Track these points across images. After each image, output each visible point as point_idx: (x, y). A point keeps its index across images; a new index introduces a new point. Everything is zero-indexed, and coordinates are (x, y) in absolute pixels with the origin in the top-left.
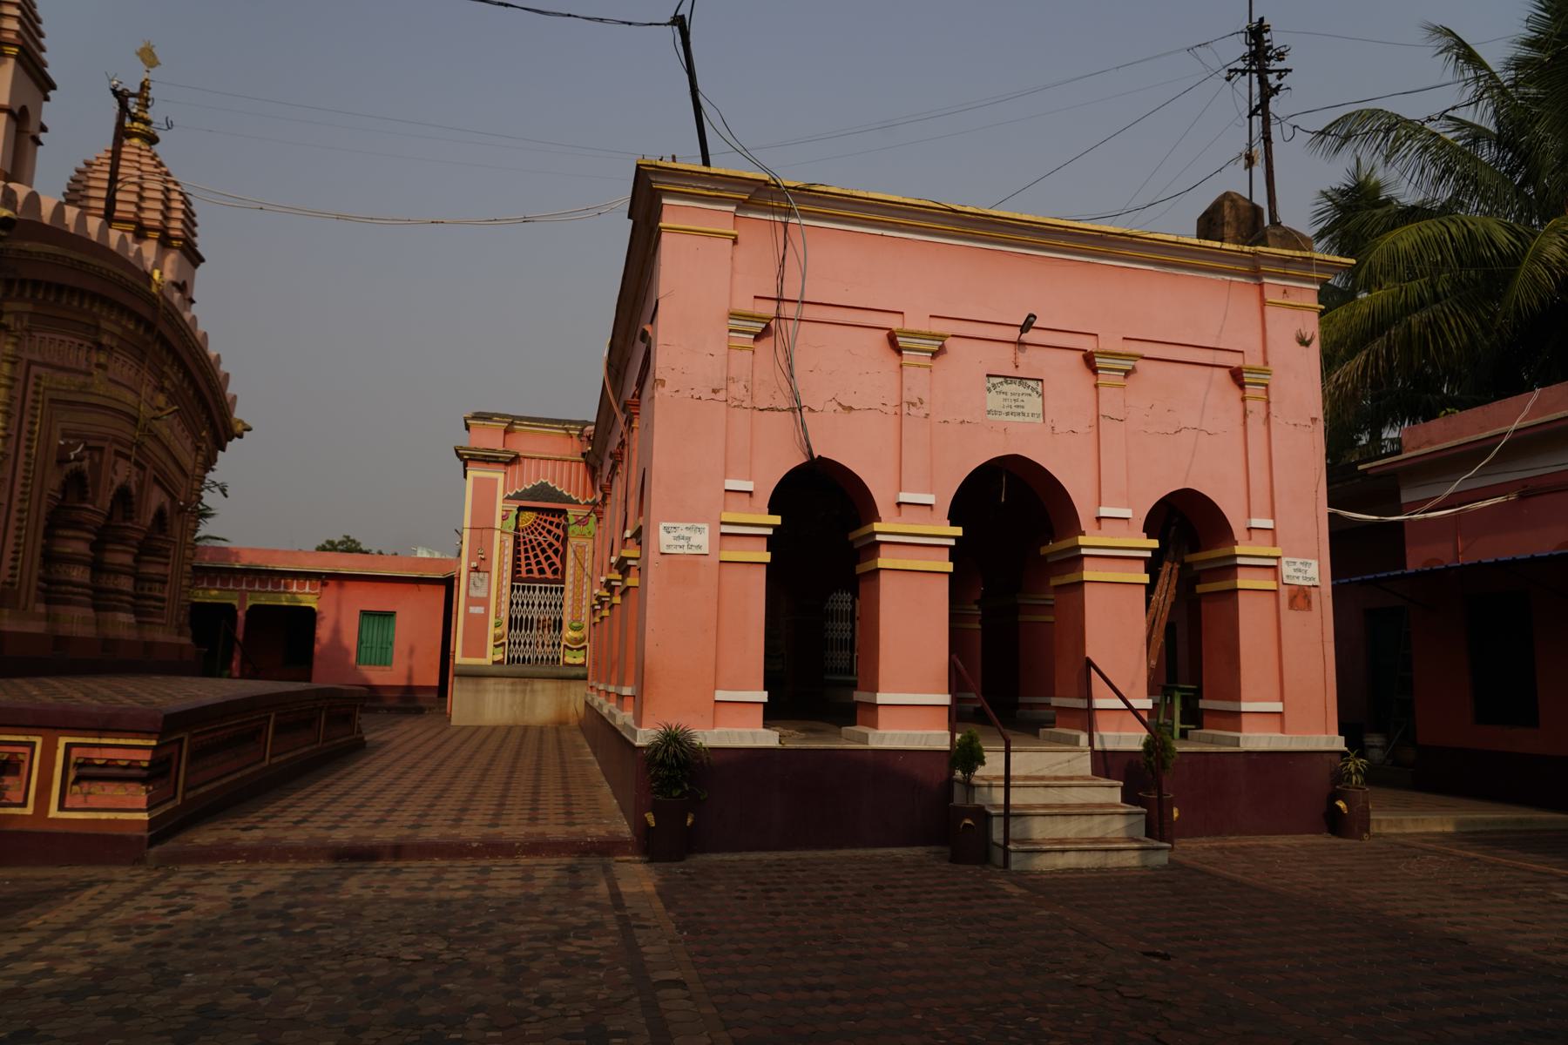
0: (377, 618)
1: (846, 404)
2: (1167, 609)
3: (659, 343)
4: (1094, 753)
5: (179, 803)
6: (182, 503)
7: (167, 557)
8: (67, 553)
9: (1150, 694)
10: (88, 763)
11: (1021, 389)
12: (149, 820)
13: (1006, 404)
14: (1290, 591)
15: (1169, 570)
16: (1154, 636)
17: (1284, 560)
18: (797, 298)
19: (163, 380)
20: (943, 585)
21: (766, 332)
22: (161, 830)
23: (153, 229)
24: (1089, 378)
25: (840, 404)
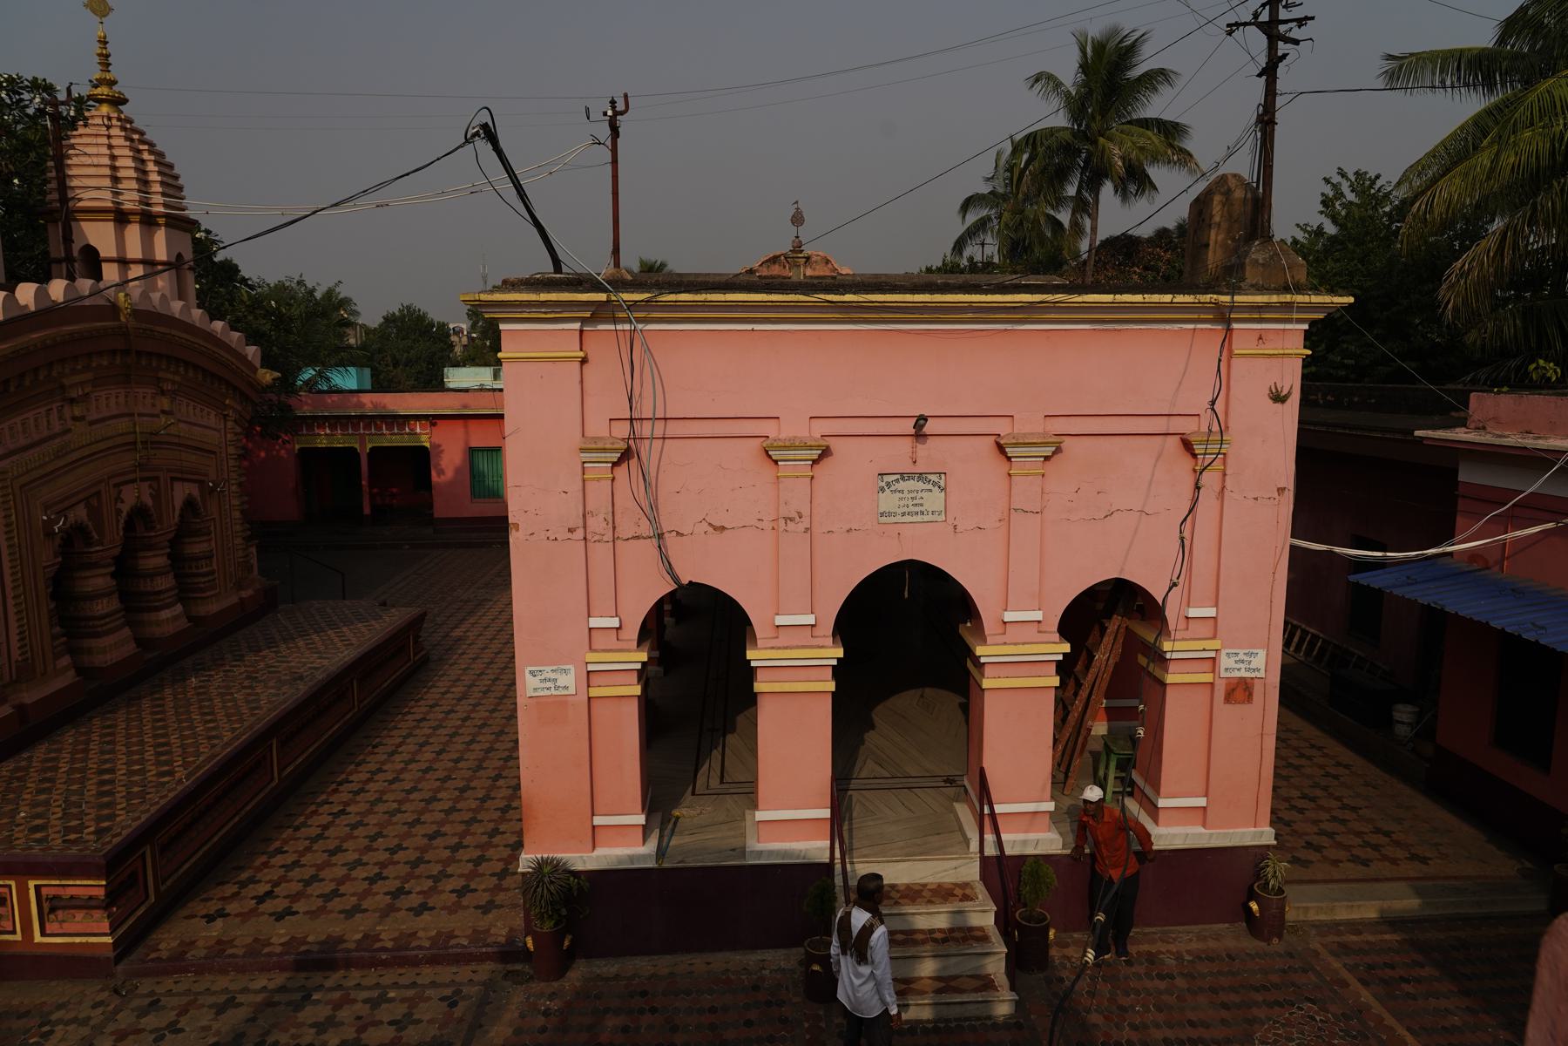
0: (485, 453)
4: (985, 861)
5: (153, 900)
6: (211, 484)
7: (210, 534)
8: (88, 592)
9: (1053, 798)
10: (56, 897)
11: (920, 485)
12: (113, 943)
13: (902, 503)
15: (1116, 627)
16: (1093, 697)
17: (1223, 653)
18: (651, 416)
19: (161, 385)
21: (626, 455)
22: (126, 945)
23: (133, 213)
24: (1002, 466)
25: (710, 524)
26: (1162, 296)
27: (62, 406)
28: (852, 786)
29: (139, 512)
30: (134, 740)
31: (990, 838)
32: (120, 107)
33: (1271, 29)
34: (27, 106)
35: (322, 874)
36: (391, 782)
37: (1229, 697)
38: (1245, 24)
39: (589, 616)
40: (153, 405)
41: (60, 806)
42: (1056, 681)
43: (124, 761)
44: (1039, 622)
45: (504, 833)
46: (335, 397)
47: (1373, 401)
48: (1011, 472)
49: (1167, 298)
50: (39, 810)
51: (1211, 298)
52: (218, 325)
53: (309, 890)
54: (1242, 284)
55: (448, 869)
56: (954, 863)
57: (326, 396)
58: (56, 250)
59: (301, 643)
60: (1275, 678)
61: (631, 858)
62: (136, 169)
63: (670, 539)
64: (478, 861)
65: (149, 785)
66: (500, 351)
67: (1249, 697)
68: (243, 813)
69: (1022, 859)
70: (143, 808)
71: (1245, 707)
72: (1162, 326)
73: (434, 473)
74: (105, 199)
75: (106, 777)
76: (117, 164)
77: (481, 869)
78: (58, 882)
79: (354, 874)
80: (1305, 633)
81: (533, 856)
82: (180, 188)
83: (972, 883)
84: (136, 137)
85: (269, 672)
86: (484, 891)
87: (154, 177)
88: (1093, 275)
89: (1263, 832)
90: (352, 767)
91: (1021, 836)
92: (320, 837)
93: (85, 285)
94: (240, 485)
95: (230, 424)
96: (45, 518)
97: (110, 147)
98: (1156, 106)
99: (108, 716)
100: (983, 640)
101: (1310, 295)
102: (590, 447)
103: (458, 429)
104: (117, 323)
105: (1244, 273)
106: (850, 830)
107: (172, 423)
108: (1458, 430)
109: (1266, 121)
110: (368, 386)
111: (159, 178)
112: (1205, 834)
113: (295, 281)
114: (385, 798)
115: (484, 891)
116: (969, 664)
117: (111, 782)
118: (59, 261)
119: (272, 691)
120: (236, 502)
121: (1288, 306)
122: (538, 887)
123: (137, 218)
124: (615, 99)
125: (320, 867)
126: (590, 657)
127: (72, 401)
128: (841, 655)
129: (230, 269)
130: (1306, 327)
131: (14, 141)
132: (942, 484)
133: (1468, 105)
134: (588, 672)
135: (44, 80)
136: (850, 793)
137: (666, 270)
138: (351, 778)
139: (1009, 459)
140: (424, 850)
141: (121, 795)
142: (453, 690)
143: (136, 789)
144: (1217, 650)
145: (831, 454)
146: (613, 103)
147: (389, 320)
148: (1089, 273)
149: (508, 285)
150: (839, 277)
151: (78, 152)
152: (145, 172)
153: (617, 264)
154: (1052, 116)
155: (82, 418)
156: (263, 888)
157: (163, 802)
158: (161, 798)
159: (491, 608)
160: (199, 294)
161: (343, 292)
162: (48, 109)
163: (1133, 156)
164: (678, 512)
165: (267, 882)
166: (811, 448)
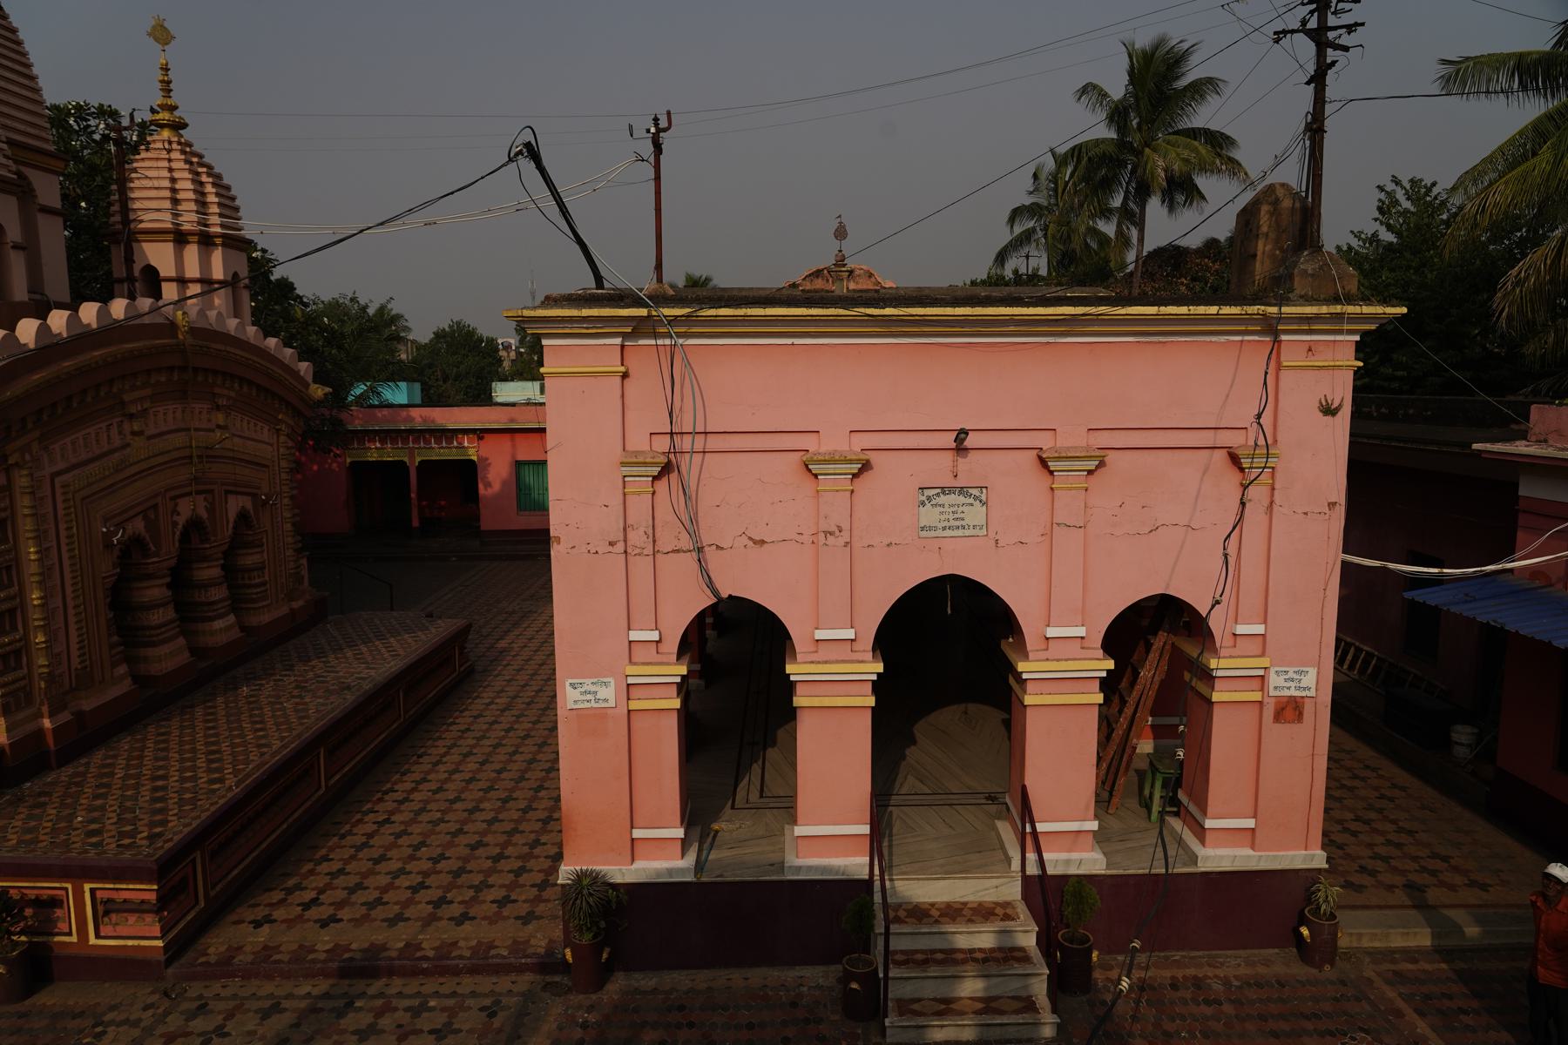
1: (757, 538)
2: (1156, 686)
3: (550, 499)
4: (1027, 880)
5: (203, 905)
6: (263, 497)
7: (263, 545)
9: (1096, 817)
10: (110, 901)
11: (962, 499)
13: (943, 517)
14: (1276, 703)
16: (1138, 714)
17: (1273, 670)
19: (216, 400)
20: (866, 720)
21: (667, 469)
22: (175, 950)
23: (192, 233)
25: (750, 538)
26: (1207, 308)
27: (122, 421)
28: (892, 802)
29: (194, 525)
30: (187, 747)
31: (1031, 856)
32: (181, 132)
33: (1319, 37)
34: (94, 132)
35: (366, 883)
36: (435, 792)
37: (1279, 716)
38: (1293, 32)
39: (629, 629)
40: (209, 420)
41: (115, 811)
42: (1099, 698)
43: (177, 768)
44: (1082, 638)
45: (544, 844)
46: (385, 412)
47: (1429, 413)
48: (1053, 486)
49: (1213, 310)
50: (96, 814)
51: (1259, 309)
52: (272, 342)
53: (354, 898)
54: (1290, 295)
55: (489, 880)
56: (995, 882)
57: (377, 411)
58: (119, 271)
59: (349, 654)
60: (1326, 697)
61: (670, 872)
62: (195, 191)
63: (710, 553)
64: (518, 872)
65: (200, 792)
66: (543, 366)
67: (1300, 717)
68: (290, 820)
69: (1064, 878)
70: (194, 814)
71: (1296, 727)
72: (1207, 339)
73: (481, 486)
74: (165, 220)
75: (160, 783)
76: (177, 186)
77: (521, 880)
78: (111, 886)
79: (397, 882)
80: (1358, 650)
81: (572, 868)
82: (237, 209)
83: (1014, 903)
84: (195, 160)
85: (318, 682)
86: (524, 901)
87: (212, 199)
88: (1140, 286)
89: (1314, 855)
90: (398, 776)
91: (1064, 856)
92: (365, 845)
93: (145, 303)
94: (292, 498)
95: (282, 438)
96: (104, 530)
97: (171, 170)
98: (1204, 116)
99: (163, 723)
100: (1025, 656)
101: (1361, 306)
102: (631, 460)
103: (505, 443)
104: (174, 341)
105: (1293, 284)
106: (890, 846)
107: (227, 438)
108: (1518, 443)
109: (1315, 129)
110: (418, 400)
111: (216, 200)
112: (1254, 856)
113: (349, 298)
114: (429, 807)
115: (524, 901)
116: (1012, 681)
117: (164, 788)
118: (120, 281)
119: (321, 700)
120: (287, 514)
121: (1339, 317)
122: (576, 900)
123: (196, 238)
124: (659, 116)
125: (365, 876)
126: (630, 670)
127: (132, 416)
128: (881, 670)
129: (286, 287)
130: (1357, 338)
131: (81, 166)
132: (984, 498)
133: (1529, 109)
134: (628, 685)
135: (110, 106)
136: (890, 808)
137: (711, 284)
138: (396, 788)
139: (1051, 473)
140: (466, 860)
141: (173, 801)
142: (497, 701)
143: (188, 796)
144: (1265, 668)
145: (871, 468)
146: (656, 120)
147: (440, 335)
148: (1136, 285)
149: (550, 301)
150: (883, 291)
151: (139, 175)
152: (204, 194)
153: (660, 280)
154: (1095, 127)
155: (140, 433)
156: (309, 895)
157: (213, 809)
158: (212, 804)
159: (535, 620)
160: (255, 312)
161: (395, 308)
162: (112, 134)
163: (1176, 167)
164: (719, 526)
165: (313, 889)
166: (851, 462)
